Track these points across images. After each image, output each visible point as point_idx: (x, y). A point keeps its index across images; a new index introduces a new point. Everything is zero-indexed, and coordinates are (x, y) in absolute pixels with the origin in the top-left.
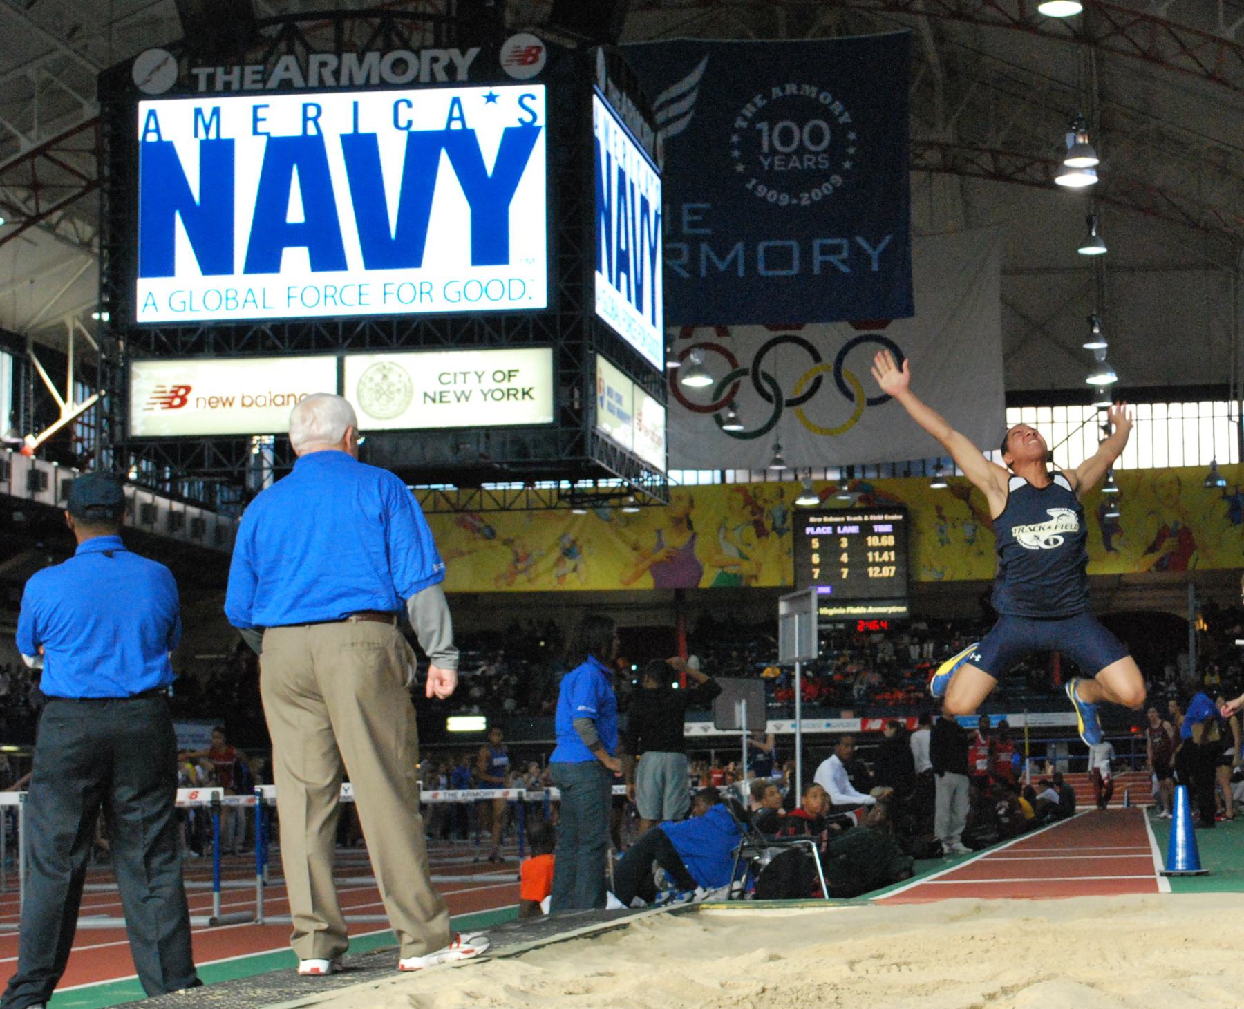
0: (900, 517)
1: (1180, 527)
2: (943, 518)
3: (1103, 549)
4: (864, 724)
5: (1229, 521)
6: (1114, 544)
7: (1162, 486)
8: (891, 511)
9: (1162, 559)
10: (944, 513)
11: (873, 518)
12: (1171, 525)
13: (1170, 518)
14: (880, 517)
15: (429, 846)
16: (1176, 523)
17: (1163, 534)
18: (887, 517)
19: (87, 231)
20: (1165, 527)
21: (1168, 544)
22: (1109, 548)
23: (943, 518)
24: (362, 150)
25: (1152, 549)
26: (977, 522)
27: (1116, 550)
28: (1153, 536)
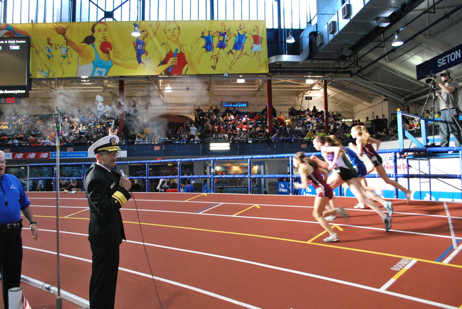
0: (24, 42)
1: (178, 52)
2: (51, 45)
3: (136, 62)
4: (13, 156)
5: (205, 49)
6: (143, 60)
7: (170, 30)
8: (20, 39)
9: (168, 69)
10: (51, 42)
11: (10, 42)
12: (174, 51)
13: (174, 48)
14: (14, 42)
15: (126, 113)
16: (177, 50)
17: (170, 55)
18: (17, 42)
19: (331, 186)
20: (171, 52)
21: (172, 61)
22: (140, 62)
23: (51, 45)
24: (327, 235)
25: (164, 62)
26: (69, 47)
27: (143, 63)
28: (164, 57)
